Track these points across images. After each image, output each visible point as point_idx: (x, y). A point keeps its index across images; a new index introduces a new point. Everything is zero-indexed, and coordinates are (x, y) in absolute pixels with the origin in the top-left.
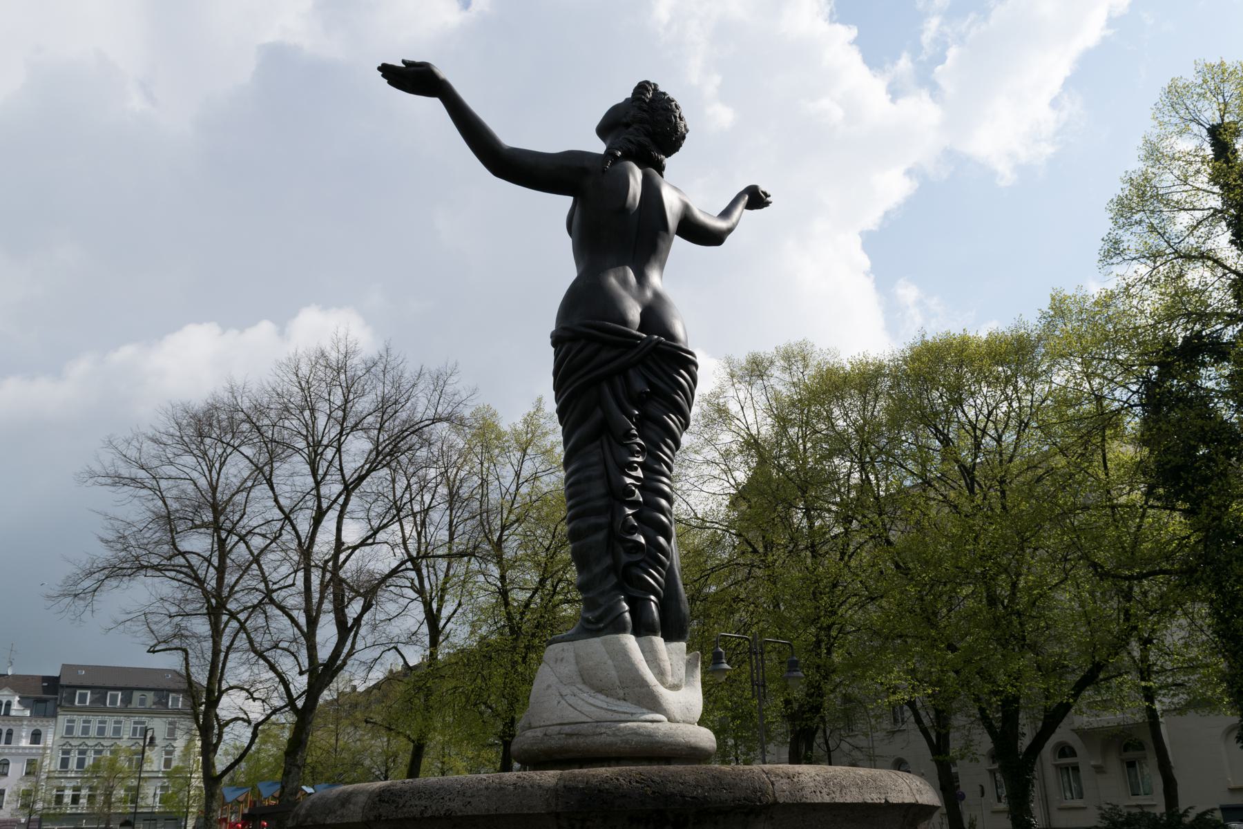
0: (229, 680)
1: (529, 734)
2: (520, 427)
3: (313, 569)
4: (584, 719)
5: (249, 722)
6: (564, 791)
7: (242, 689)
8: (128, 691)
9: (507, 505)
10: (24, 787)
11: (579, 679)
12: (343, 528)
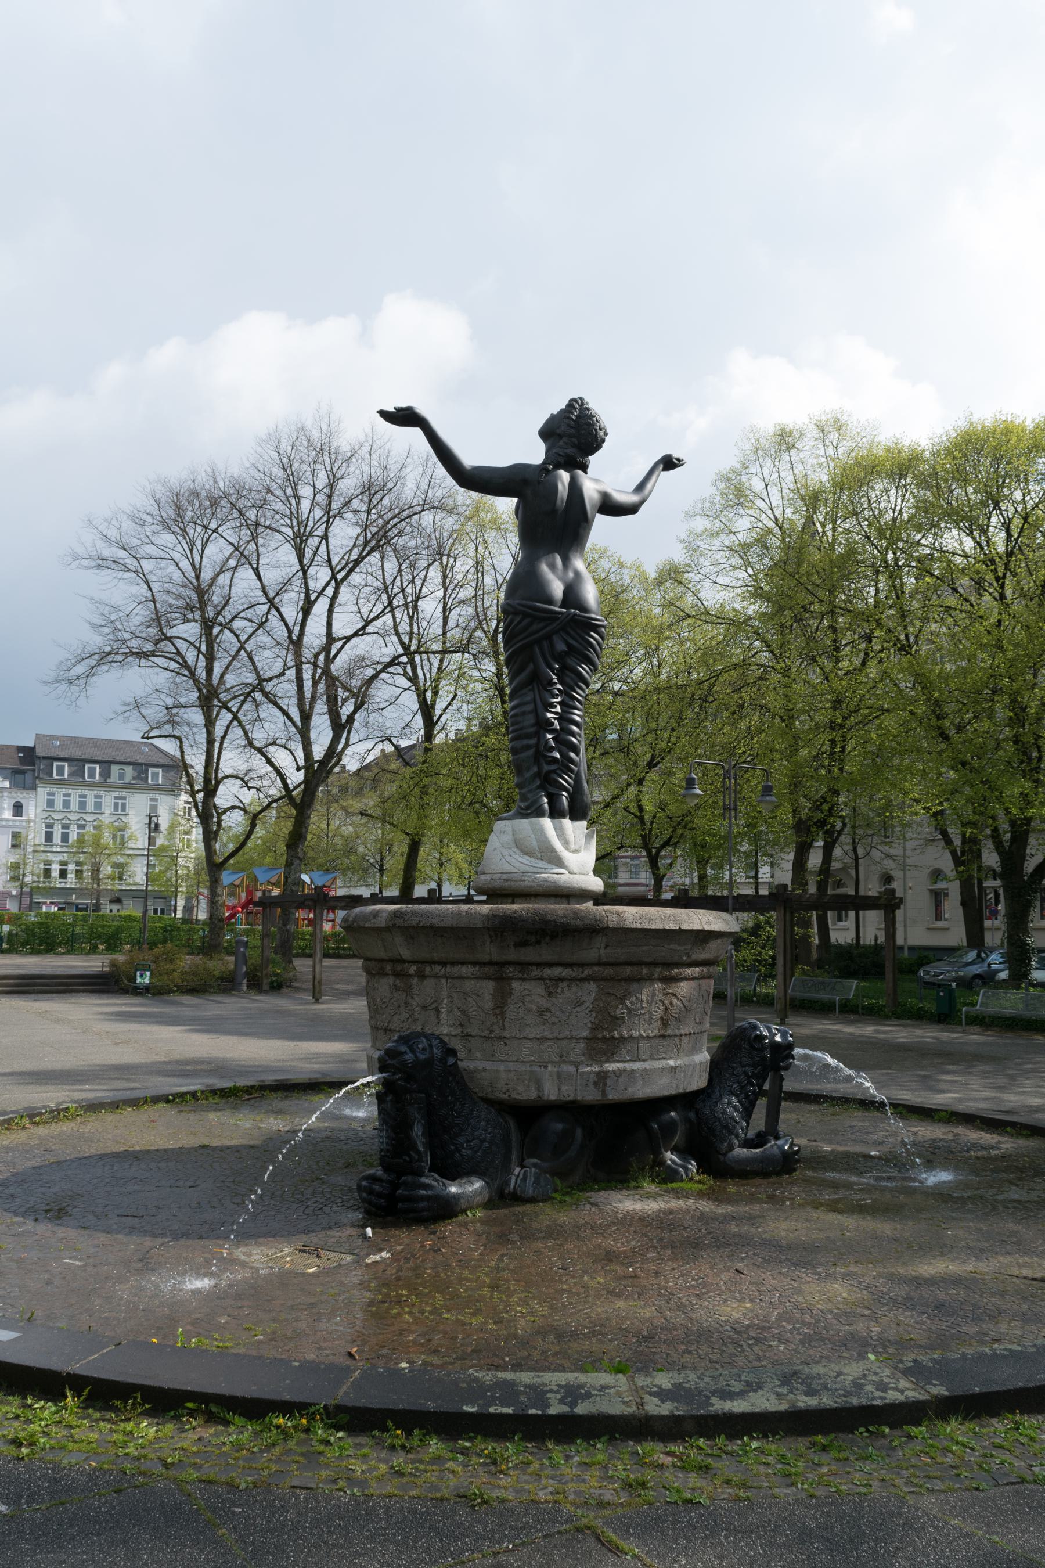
3: (305, 667)
6: (493, 916)
7: (237, 777)
8: (106, 764)
10: (13, 858)
12: (334, 622)
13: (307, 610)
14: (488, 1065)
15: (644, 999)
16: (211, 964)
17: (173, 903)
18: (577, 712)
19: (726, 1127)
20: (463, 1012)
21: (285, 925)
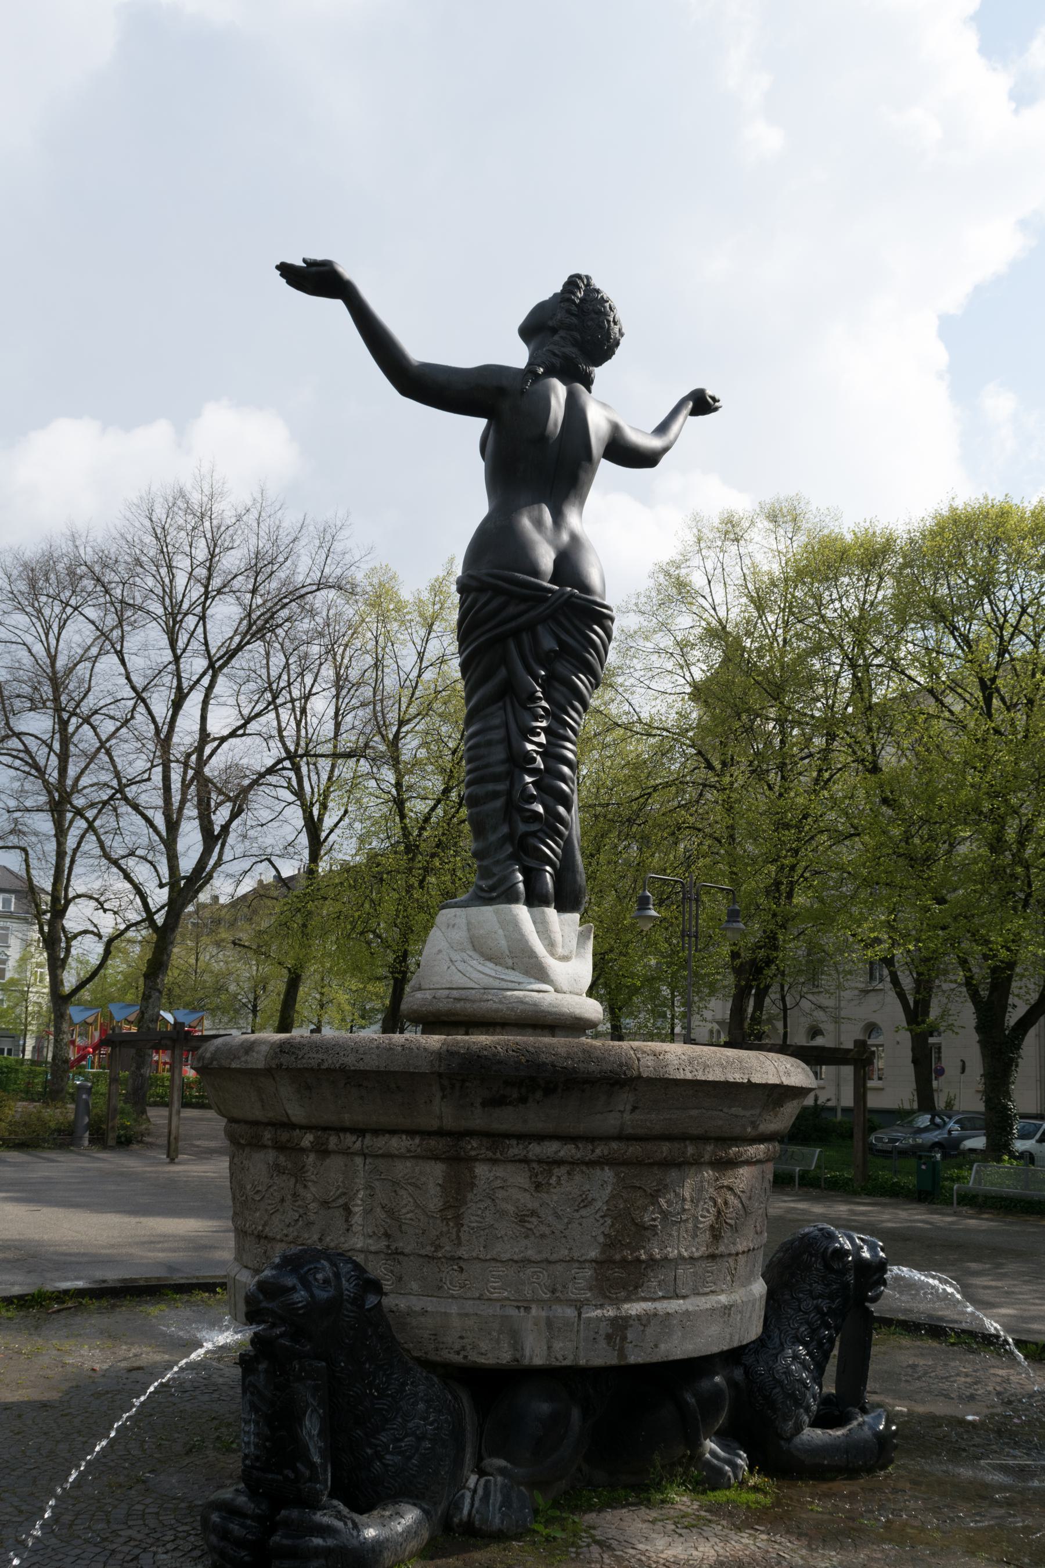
0: (78, 886)
1: (419, 995)
2: (426, 596)
4: (472, 985)
5: (99, 936)
6: (447, 1055)
7: (91, 898)
9: (407, 692)
11: (470, 946)
12: (209, 715)
13: (177, 705)
14: (430, 1304)
15: (687, 1195)
16: (48, 1113)
17: (21, 1042)
18: (569, 745)
19: (792, 1396)
20: (391, 1213)
21: (139, 1068)
